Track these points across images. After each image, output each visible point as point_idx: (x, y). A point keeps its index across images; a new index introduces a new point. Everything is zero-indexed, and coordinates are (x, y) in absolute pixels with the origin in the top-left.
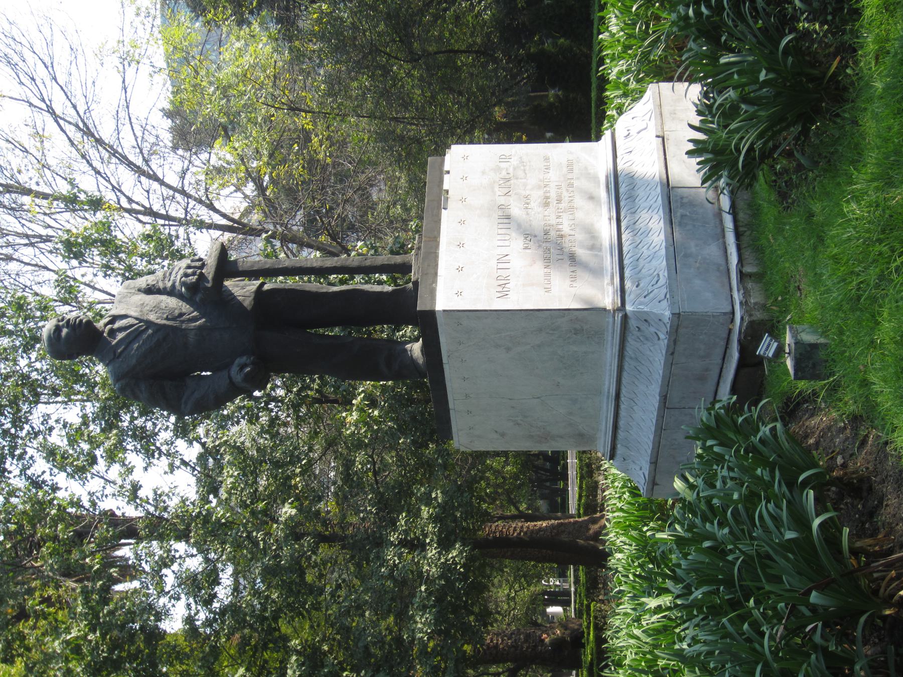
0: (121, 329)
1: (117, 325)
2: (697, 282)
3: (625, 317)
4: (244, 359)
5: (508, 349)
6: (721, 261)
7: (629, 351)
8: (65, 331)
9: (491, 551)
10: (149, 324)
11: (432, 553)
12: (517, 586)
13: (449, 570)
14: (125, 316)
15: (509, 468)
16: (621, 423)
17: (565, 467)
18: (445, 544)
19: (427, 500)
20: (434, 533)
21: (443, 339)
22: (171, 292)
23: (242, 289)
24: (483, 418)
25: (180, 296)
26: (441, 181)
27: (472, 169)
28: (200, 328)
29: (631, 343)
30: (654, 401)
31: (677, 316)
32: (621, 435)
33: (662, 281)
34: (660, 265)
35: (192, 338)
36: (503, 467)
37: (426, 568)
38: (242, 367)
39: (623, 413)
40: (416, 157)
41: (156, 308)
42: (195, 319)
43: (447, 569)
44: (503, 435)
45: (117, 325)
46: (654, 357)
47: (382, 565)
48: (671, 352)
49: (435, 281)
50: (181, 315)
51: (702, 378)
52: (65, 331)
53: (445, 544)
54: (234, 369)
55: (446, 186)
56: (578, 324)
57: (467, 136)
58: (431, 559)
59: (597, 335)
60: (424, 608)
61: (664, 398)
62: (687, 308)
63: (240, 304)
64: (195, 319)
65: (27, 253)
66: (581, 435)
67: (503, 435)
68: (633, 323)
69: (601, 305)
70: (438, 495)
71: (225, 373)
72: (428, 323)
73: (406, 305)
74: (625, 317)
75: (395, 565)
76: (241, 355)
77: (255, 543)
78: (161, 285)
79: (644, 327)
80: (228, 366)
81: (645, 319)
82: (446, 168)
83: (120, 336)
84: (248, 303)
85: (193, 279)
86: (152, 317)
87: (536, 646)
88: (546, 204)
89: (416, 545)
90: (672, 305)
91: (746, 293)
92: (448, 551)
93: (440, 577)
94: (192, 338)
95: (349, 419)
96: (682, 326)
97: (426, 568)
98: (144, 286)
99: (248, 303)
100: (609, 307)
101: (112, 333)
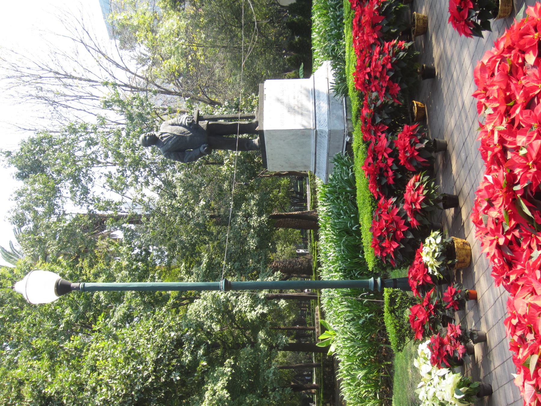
0: (165, 137)
1: (163, 135)
2: (336, 121)
3: (316, 131)
4: (205, 145)
5: (284, 140)
6: (342, 115)
7: (318, 141)
8: (147, 138)
9: (276, 221)
10: (174, 135)
11: (255, 218)
12: (285, 246)
13: (262, 224)
14: (166, 133)
15: (280, 194)
16: (317, 162)
17: (306, 196)
18: (260, 215)
19: (253, 198)
20: (256, 210)
21: (265, 138)
22: (181, 125)
23: (203, 124)
24: (277, 161)
25: (185, 126)
26: (263, 91)
27: (272, 88)
28: (190, 136)
29: (318, 138)
30: (326, 155)
31: (330, 131)
32: (317, 165)
33: (326, 121)
34: (326, 116)
35: (188, 139)
36: (278, 193)
37: (252, 223)
38: (204, 148)
39: (317, 159)
40: (254, 84)
41: (176, 130)
42: (189, 133)
43: (261, 224)
44: (282, 166)
45: (163, 135)
46: (325, 142)
47: (236, 224)
48: (329, 141)
49: (263, 121)
50: (184, 132)
51: (338, 148)
52: (147, 138)
53: (260, 215)
54: (201, 149)
55: (265, 93)
56: (303, 134)
57: (269, 77)
58: (254, 221)
59: (309, 136)
60: (253, 237)
61: (328, 154)
62: (332, 128)
63: (202, 129)
64: (189, 133)
65: (75, 104)
66: (305, 166)
67: (282, 166)
68: (318, 133)
69: (309, 127)
70: (256, 196)
71: (198, 149)
72: (261, 133)
73: (252, 129)
74: (316, 131)
75: (241, 223)
76: (204, 144)
77: (189, 217)
78: (177, 123)
79: (321, 134)
80: (199, 147)
81: (322, 132)
82: (265, 87)
83: (165, 139)
84: (205, 128)
85: (191, 121)
86: (175, 133)
87: (293, 266)
88: (294, 98)
89: (248, 216)
90: (328, 128)
91: (348, 124)
92: (260, 217)
93: (258, 227)
94: (188, 139)
95: (224, 169)
96: (331, 133)
97: (252, 223)
98: (171, 123)
99: (205, 128)
100: (312, 128)
101: (162, 138)
